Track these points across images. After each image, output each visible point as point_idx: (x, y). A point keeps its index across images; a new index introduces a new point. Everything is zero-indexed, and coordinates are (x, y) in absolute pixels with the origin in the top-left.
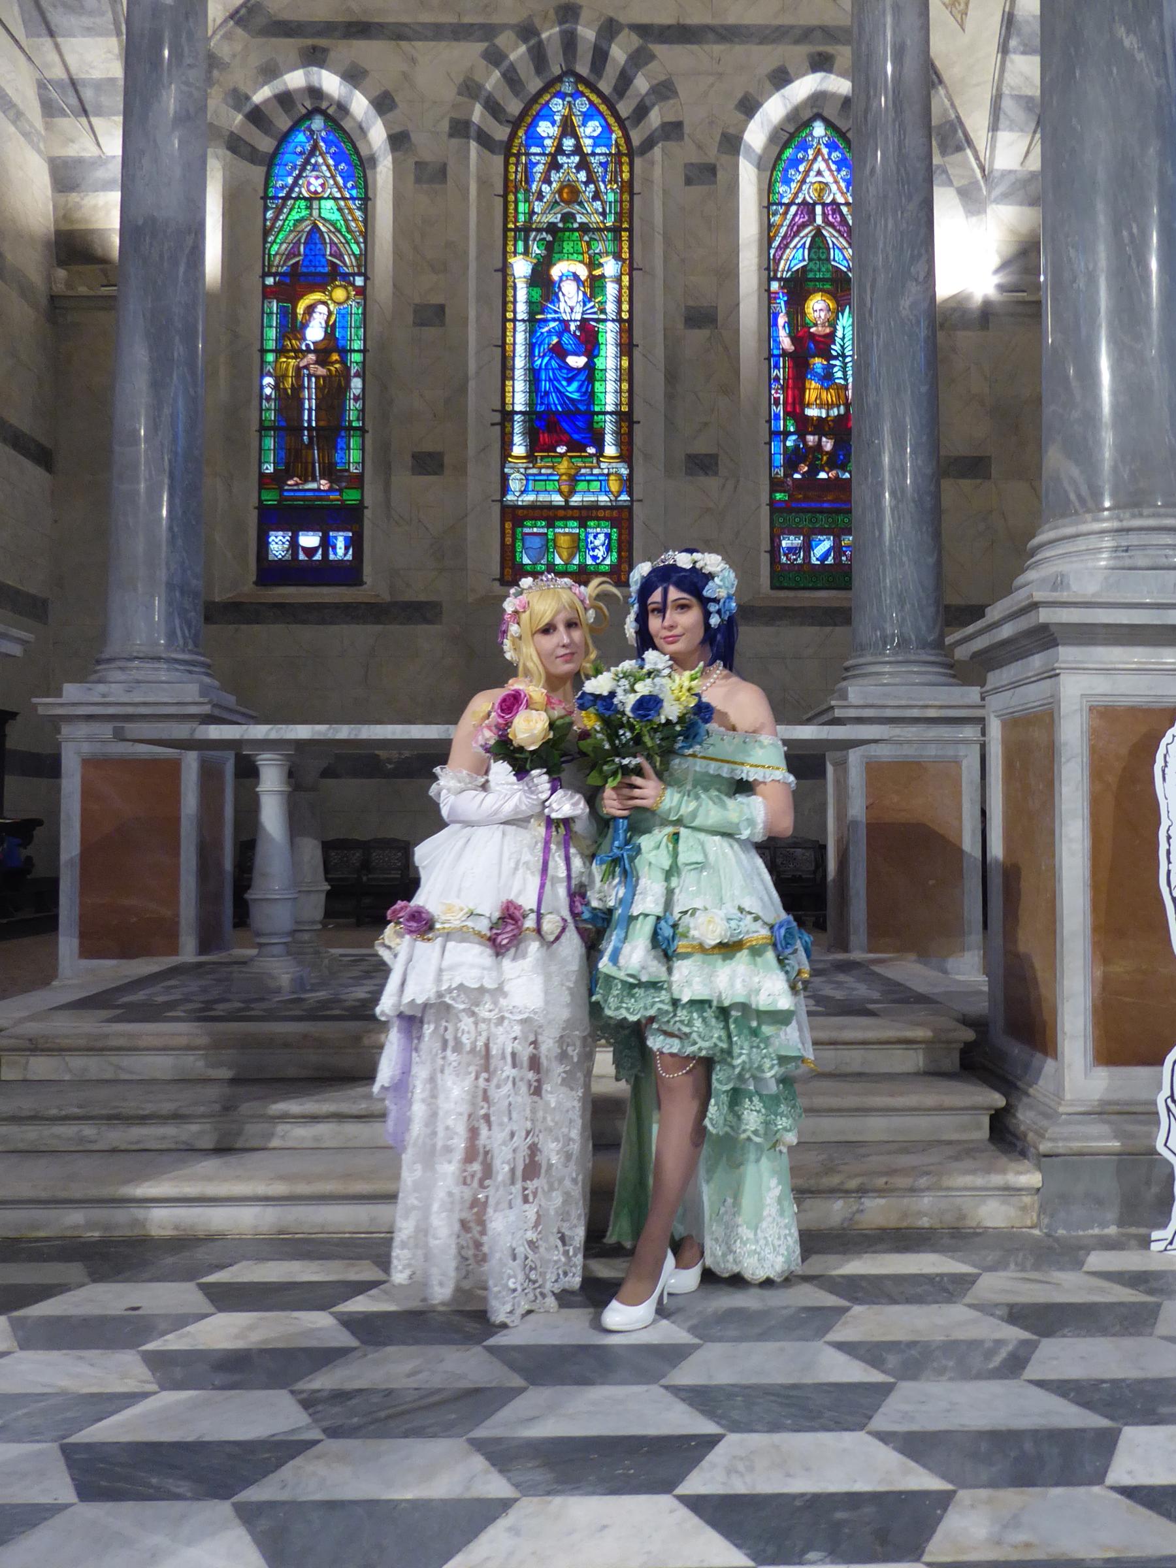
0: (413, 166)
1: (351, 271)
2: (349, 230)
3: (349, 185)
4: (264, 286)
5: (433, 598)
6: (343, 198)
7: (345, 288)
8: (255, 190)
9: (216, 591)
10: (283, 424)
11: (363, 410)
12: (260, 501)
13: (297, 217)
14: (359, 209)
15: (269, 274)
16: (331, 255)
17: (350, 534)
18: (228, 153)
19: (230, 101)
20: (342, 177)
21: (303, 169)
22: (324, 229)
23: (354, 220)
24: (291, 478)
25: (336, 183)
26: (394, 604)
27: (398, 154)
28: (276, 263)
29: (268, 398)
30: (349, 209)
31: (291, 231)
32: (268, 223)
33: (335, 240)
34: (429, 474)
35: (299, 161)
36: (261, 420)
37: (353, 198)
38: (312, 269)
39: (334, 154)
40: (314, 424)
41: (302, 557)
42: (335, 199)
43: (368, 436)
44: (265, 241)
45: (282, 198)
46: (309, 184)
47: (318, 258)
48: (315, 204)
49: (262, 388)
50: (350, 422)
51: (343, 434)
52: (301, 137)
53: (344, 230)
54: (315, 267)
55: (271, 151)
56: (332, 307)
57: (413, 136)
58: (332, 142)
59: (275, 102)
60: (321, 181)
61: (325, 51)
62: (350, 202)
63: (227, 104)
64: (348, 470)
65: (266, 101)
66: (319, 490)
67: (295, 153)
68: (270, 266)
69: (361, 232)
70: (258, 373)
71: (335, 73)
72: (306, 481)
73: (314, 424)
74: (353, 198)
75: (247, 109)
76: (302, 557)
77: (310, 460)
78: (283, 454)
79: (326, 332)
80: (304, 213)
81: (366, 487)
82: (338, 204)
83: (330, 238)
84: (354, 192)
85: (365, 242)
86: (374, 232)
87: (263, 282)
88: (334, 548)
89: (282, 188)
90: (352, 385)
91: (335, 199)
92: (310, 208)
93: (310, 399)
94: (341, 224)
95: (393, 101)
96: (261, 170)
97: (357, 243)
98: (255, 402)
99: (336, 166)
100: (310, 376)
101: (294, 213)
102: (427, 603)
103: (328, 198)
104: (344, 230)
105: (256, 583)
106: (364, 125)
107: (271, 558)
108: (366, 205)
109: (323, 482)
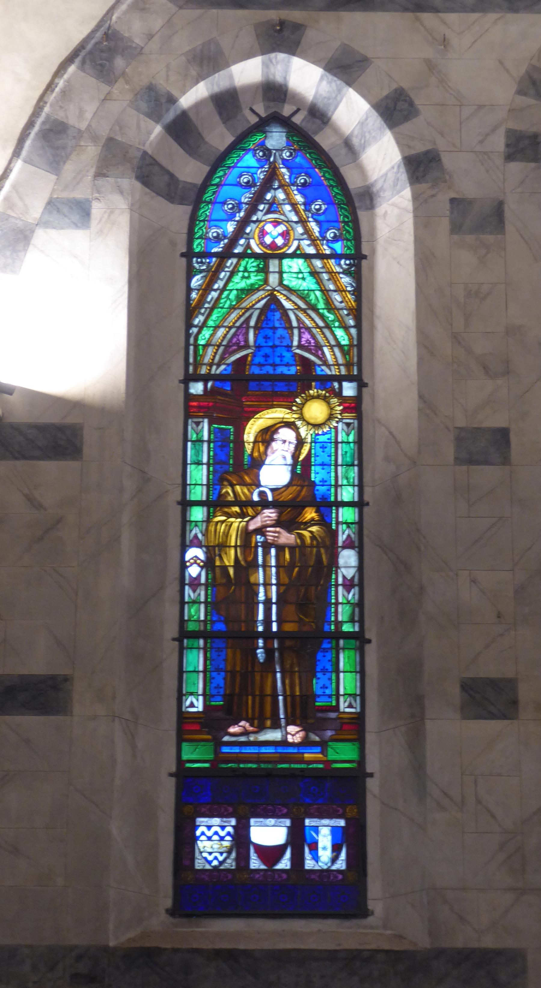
0: (448, 206)
1: (334, 371)
2: (330, 306)
3: (330, 235)
4: (188, 397)
5: (509, 943)
6: (320, 256)
7: (325, 399)
8: (173, 244)
9: (111, 927)
10: (221, 626)
11: (360, 604)
12: (180, 762)
13: (243, 284)
14: (346, 272)
15: (196, 378)
16: (300, 346)
17: (342, 823)
18: (138, 185)
19: (143, 105)
20: (319, 223)
21: (253, 209)
22: (287, 305)
23: (339, 290)
24: (236, 722)
25: (308, 232)
26: (439, 953)
27: (423, 186)
28: (207, 360)
29: (195, 583)
30: (330, 273)
31: (232, 308)
32: (194, 295)
33: (308, 323)
34: (492, 716)
35: (246, 197)
36: (182, 622)
37: (335, 256)
38: (269, 370)
39: (304, 185)
40: (275, 628)
41: (255, 863)
42: (307, 257)
43: (371, 650)
44: (189, 325)
45: (216, 255)
46: (263, 233)
47: (279, 351)
48: (273, 265)
49: (183, 566)
50: (338, 624)
51: (325, 645)
52: (249, 160)
53: (321, 305)
54: (274, 365)
55: (199, 180)
56: (303, 431)
57: (447, 160)
58: (301, 167)
59: (211, 106)
60: (281, 228)
61: (298, 28)
62: (332, 262)
63: (138, 109)
64: (336, 708)
65: (199, 105)
66: (284, 743)
67: (239, 184)
68: (197, 365)
69: (350, 310)
70: (178, 541)
71: (316, 62)
72: (261, 728)
73: (275, 628)
74: (335, 256)
75: (170, 116)
76: (255, 863)
77: (268, 690)
78: (220, 679)
79: (293, 472)
80: (255, 279)
81: (370, 738)
82: (310, 265)
83: (298, 320)
84: (338, 247)
85: (358, 326)
86: (372, 311)
87: (187, 389)
88: (314, 847)
89: (218, 239)
90: (341, 562)
91: (307, 257)
92: (265, 270)
93: (267, 584)
94: (317, 297)
95: (411, 104)
96: (185, 211)
97: (346, 328)
98: (172, 590)
99: (307, 204)
100: (267, 546)
101: (237, 278)
102: (499, 953)
103: (294, 255)
104: (321, 305)
105: (172, 912)
106: (355, 141)
107: (199, 864)
108: (359, 267)
109: (292, 729)
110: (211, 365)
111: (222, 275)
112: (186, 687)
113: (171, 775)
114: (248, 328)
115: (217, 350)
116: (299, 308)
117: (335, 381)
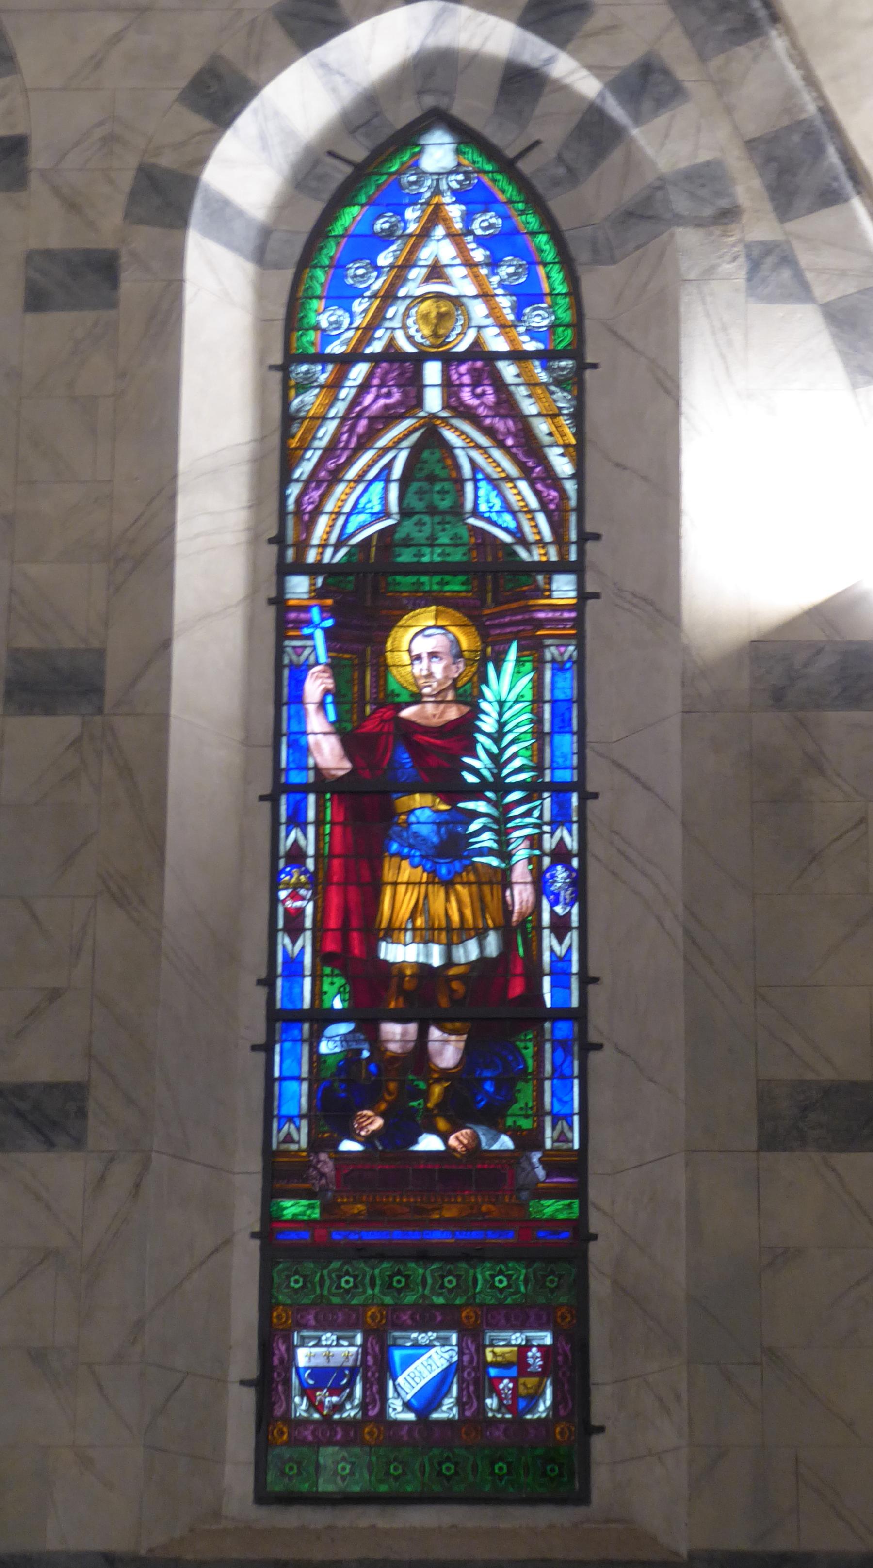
1: (537, 555)
15: (300, 568)
68: (302, 546)
110: (323, 546)
111: (343, 394)
112: (279, 1106)
113: (254, 1235)
114: (388, 481)
115: (335, 520)
116: (478, 447)
117: (540, 572)
